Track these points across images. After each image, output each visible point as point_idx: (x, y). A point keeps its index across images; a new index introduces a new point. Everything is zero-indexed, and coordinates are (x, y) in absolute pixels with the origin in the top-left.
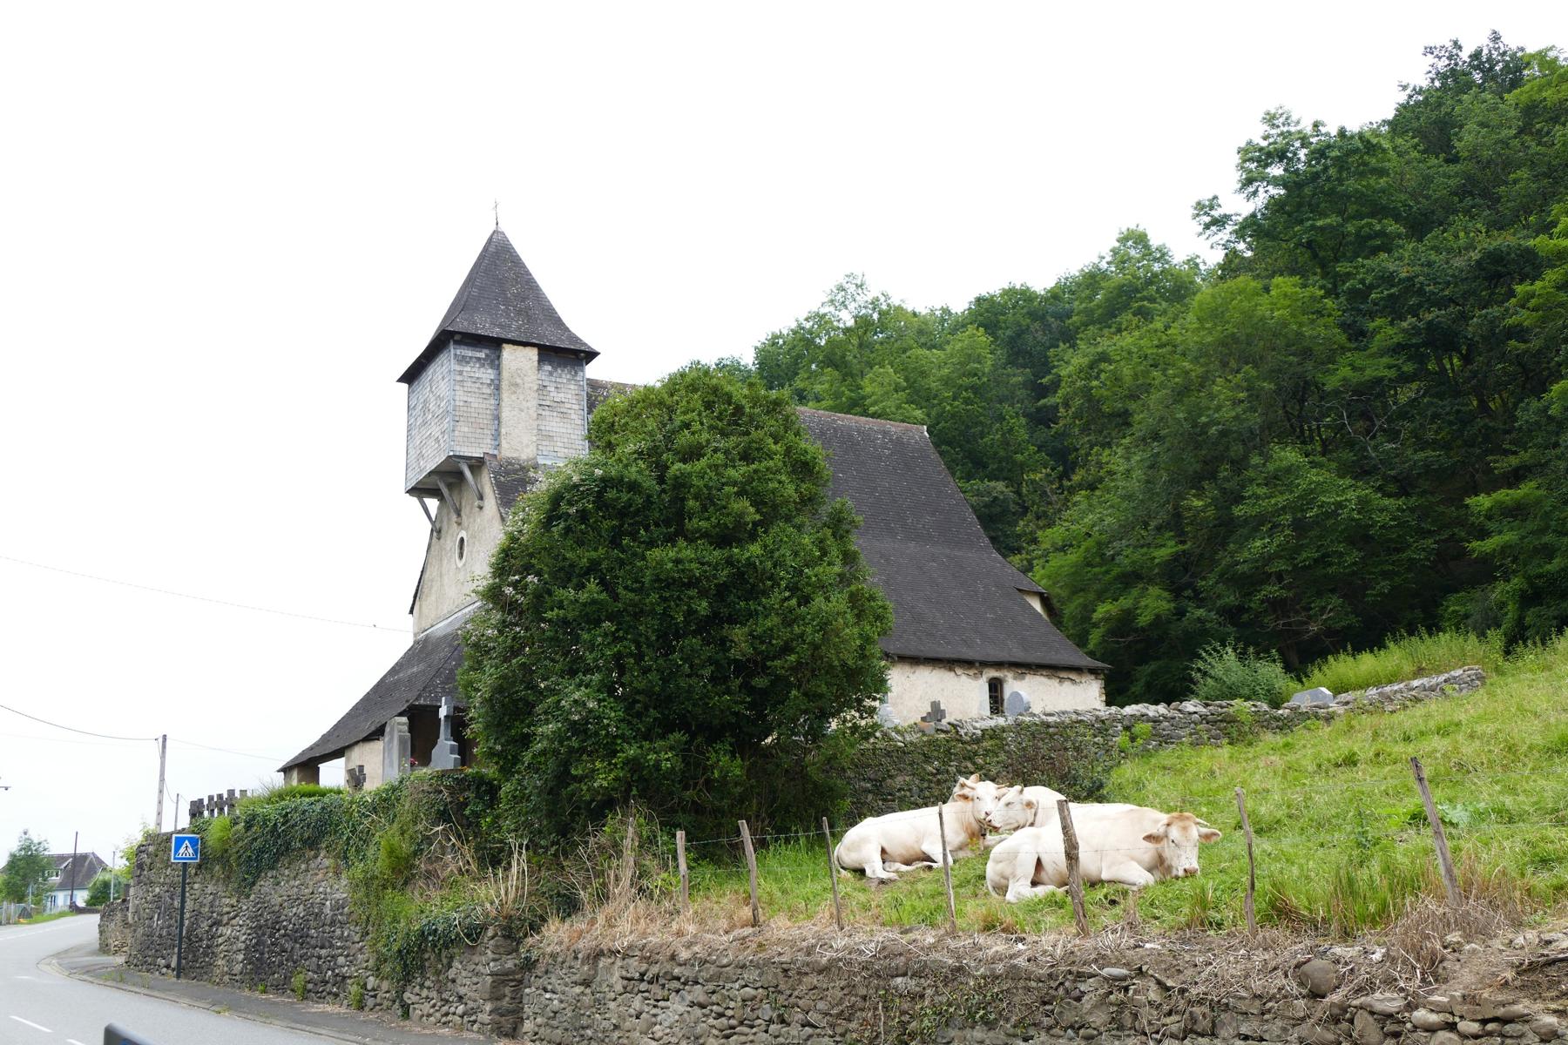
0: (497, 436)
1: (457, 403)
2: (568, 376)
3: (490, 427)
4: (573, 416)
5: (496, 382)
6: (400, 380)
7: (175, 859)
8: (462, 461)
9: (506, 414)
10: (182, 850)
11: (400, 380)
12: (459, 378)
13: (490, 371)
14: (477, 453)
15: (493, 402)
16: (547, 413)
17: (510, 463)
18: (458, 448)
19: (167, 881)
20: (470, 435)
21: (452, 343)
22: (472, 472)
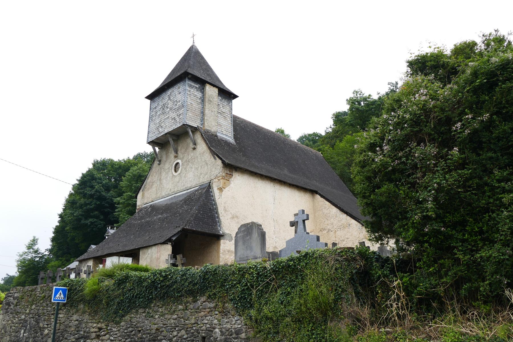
0: (203, 120)
1: (188, 103)
2: (227, 103)
3: (200, 116)
4: (228, 119)
5: (202, 98)
6: (148, 97)
7: (54, 300)
8: (189, 127)
9: (207, 111)
10: (58, 296)
11: (148, 97)
12: (189, 93)
13: (200, 93)
14: (195, 125)
15: (201, 106)
16: (220, 115)
17: (208, 132)
18: (188, 122)
19: (32, 311)
20: (192, 117)
21: (187, 78)
22: (192, 132)
